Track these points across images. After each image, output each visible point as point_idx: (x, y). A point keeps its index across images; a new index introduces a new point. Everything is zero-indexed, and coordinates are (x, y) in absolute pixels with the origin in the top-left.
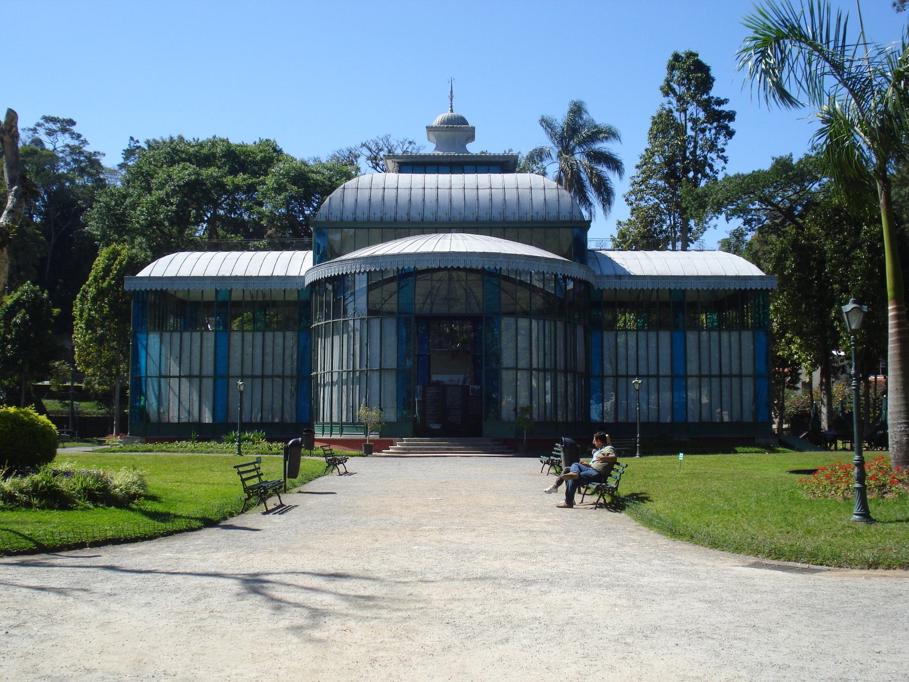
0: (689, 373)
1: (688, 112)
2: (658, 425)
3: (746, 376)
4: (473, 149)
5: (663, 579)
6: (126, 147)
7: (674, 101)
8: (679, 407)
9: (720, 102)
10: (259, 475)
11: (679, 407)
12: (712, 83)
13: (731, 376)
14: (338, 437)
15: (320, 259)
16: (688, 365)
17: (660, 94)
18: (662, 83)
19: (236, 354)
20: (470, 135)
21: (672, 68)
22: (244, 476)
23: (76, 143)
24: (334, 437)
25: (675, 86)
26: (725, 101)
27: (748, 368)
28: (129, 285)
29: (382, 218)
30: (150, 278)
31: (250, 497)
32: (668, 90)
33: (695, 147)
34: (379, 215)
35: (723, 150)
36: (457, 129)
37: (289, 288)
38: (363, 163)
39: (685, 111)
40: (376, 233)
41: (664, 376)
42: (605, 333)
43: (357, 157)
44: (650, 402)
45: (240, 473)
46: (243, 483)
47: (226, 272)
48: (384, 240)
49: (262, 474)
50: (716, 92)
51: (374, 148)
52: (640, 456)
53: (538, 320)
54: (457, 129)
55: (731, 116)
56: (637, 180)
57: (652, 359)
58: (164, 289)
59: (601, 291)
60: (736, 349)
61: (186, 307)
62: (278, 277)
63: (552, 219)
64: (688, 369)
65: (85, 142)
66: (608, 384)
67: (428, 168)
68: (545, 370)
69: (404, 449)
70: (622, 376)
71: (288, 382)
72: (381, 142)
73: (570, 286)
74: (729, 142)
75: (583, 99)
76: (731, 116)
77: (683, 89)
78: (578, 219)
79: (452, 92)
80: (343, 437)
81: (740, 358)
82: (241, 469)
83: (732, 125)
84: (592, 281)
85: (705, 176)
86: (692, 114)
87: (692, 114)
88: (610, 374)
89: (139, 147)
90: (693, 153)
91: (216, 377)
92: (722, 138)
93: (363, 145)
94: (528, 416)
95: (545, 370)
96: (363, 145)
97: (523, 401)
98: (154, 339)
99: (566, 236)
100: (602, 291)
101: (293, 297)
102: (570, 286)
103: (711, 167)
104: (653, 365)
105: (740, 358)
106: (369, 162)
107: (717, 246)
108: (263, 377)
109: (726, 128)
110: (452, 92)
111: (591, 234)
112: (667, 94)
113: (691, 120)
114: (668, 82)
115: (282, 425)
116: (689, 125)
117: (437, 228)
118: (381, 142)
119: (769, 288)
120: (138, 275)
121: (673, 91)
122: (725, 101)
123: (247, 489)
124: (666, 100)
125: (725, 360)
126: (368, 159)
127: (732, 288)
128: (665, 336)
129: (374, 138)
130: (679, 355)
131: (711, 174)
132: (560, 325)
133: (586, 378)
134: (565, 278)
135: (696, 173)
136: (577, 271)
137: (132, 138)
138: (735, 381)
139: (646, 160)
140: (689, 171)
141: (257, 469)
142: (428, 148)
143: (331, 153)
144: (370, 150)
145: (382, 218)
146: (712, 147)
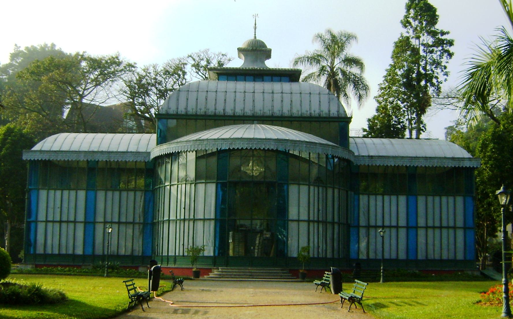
0: (419, 225)
1: (421, 39)
2: (397, 261)
3: (420, 227)
4: (270, 64)
6: (13, 52)
7: (411, 31)
8: (412, 246)
9: (443, 33)
11: (412, 246)
12: (437, 19)
13: (448, 227)
14: (173, 266)
15: (162, 140)
16: (419, 237)
17: (400, 25)
18: (402, 18)
19: (100, 205)
20: (268, 54)
24: (169, 266)
25: (411, 20)
26: (448, 33)
27: (460, 223)
28: (26, 156)
29: (205, 112)
30: (41, 151)
31: (132, 301)
32: (406, 23)
33: (426, 63)
34: (203, 110)
35: (445, 68)
36: (257, 50)
37: (139, 160)
39: (418, 38)
40: (200, 123)
41: (42, 221)
42: (361, 196)
44: (392, 245)
46: (129, 293)
47: (95, 148)
48: (206, 128)
49: (136, 288)
50: (439, 26)
51: (197, 59)
52: (384, 281)
53: (314, 186)
54: (257, 50)
55: (451, 43)
56: (383, 86)
58: (51, 159)
59: (358, 167)
60: (452, 208)
61: (64, 171)
62: (131, 152)
63: (325, 116)
66: (362, 231)
67: (238, 77)
68: (318, 222)
69: (220, 275)
70: (373, 227)
71: (137, 226)
73: (336, 160)
74: (450, 61)
76: (451, 43)
77: (417, 22)
78: (343, 116)
79: (255, 24)
80: (176, 266)
81: (455, 214)
83: (451, 49)
84: (352, 159)
85: (433, 85)
86: (424, 40)
87: (424, 40)
88: (364, 225)
90: (425, 68)
91: (86, 223)
92: (445, 57)
94: (306, 254)
95: (318, 222)
97: (303, 243)
98: (43, 193)
99: (335, 126)
100: (359, 166)
101: (143, 166)
102: (336, 160)
103: (437, 78)
105: (455, 214)
106: (194, 68)
108: (61, 222)
109: (447, 51)
110: (255, 24)
111: (351, 126)
112: (406, 27)
113: (423, 45)
114: (406, 17)
115: (132, 257)
116: (422, 48)
117: (244, 120)
118: (202, 55)
119: (475, 166)
120: (33, 149)
121: (410, 23)
122: (448, 33)
124: (406, 30)
125: (444, 217)
128: (403, 199)
130: (412, 212)
131: (436, 84)
132: (336, 191)
133: (347, 226)
134: (333, 157)
135: (426, 82)
136: (341, 153)
137: (16, 45)
138: (451, 231)
139: (391, 78)
140: (421, 81)
142: (237, 62)
143: (166, 62)
144: (194, 60)
145: (205, 112)
146: (437, 64)
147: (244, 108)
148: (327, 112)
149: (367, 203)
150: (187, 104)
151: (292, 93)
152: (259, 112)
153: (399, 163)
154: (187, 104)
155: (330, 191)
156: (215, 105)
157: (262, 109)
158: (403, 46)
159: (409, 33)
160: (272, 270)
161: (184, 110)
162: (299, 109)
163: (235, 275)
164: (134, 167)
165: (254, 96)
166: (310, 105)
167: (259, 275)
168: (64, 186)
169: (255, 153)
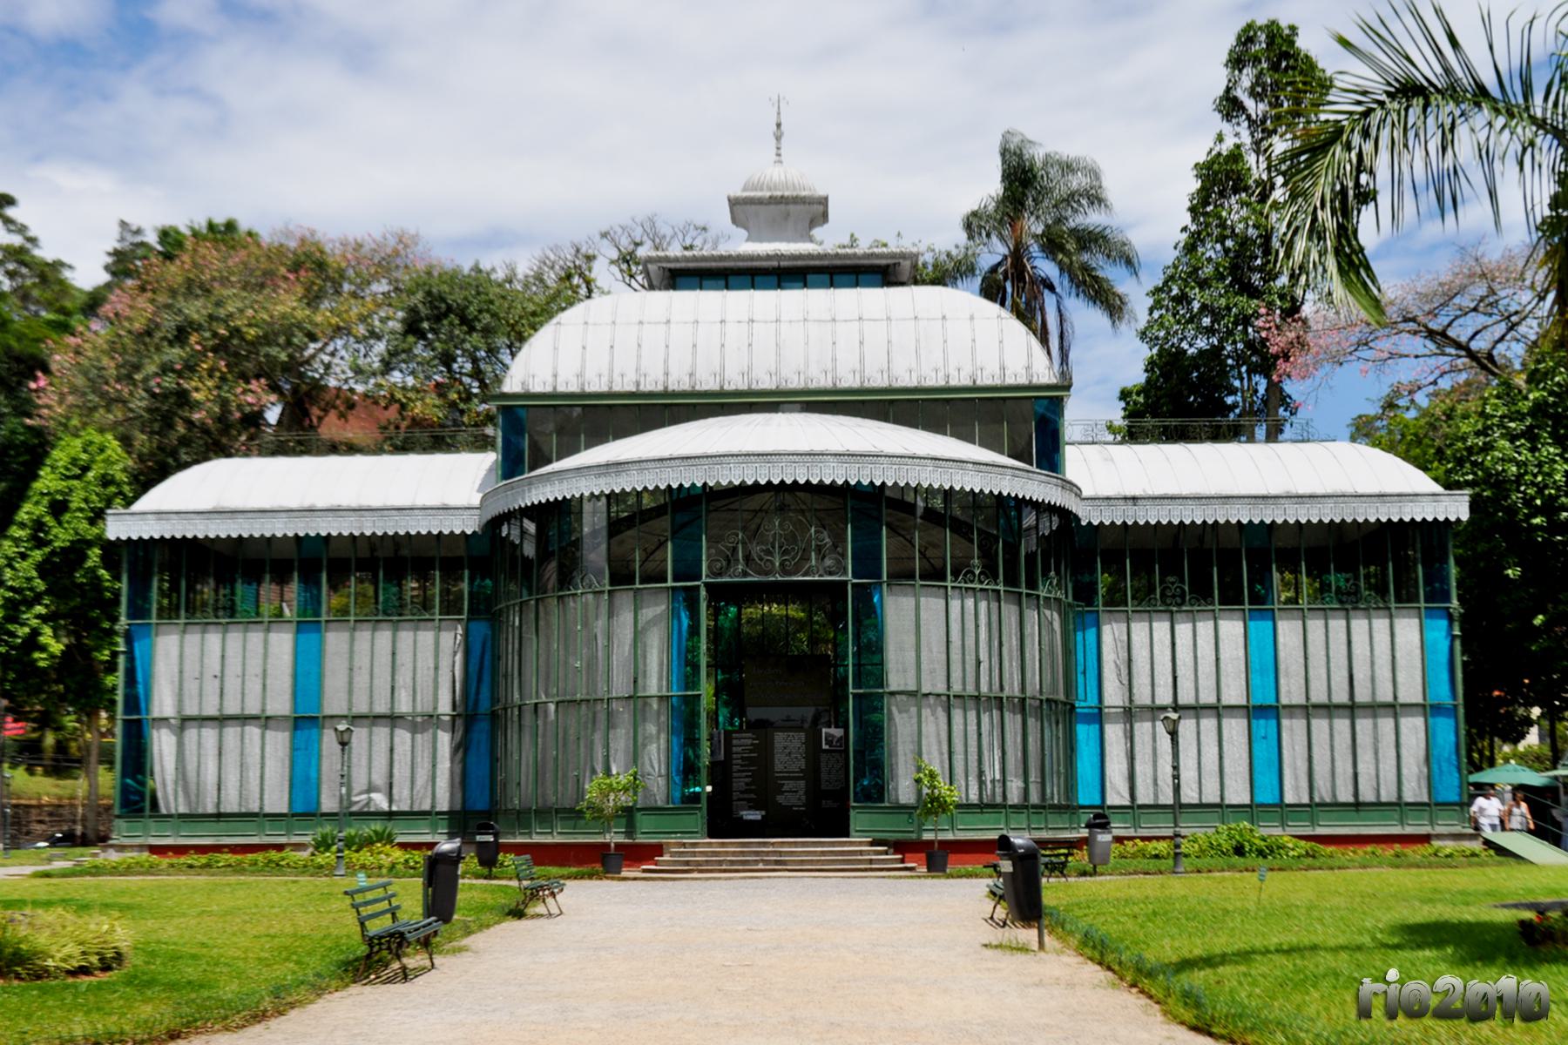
5: (154, 594)
10: (389, 898)
21: (1237, 62)
22: (365, 911)
23: (16, 240)
32: (1230, 106)
38: (604, 273)
43: (590, 258)
45: (356, 907)
46: (362, 924)
57: (1207, 665)
61: (216, 575)
64: (1414, 701)
65: (33, 240)
72: (640, 230)
75: (1272, 18)
77: (1262, 107)
82: (359, 898)
89: (143, 244)
93: (604, 235)
96: (604, 235)
104: (1207, 684)
106: (615, 269)
107: (1347, 432)
112: (1228, 117)
123: (370, 941)
124: (1227, 128)
125: (1185, 673)
126: (612, 262)
127: (1372, 520)
129: (628, 222)
141: (389, 898)
147: (750, 368)
148: (997, 371)
149: (1125, 638)
150: (583, 361)
151: (888, 319)
152: (796, 378)
153: (1220, 515)
154: (583, 361)
155: (955, 605)
156: (666, 361)
157: (829, 366)
158: (1220, 177)
159: (1238, 135)
160: (765, 844)
161: (687, 379)
162: (914, 365)
163: (732, 863)
164: (295, 556)
165: (778, 333)
166: (778, 354)
167: (802, 862)
168: (393, 612)
169: (788, 498)
